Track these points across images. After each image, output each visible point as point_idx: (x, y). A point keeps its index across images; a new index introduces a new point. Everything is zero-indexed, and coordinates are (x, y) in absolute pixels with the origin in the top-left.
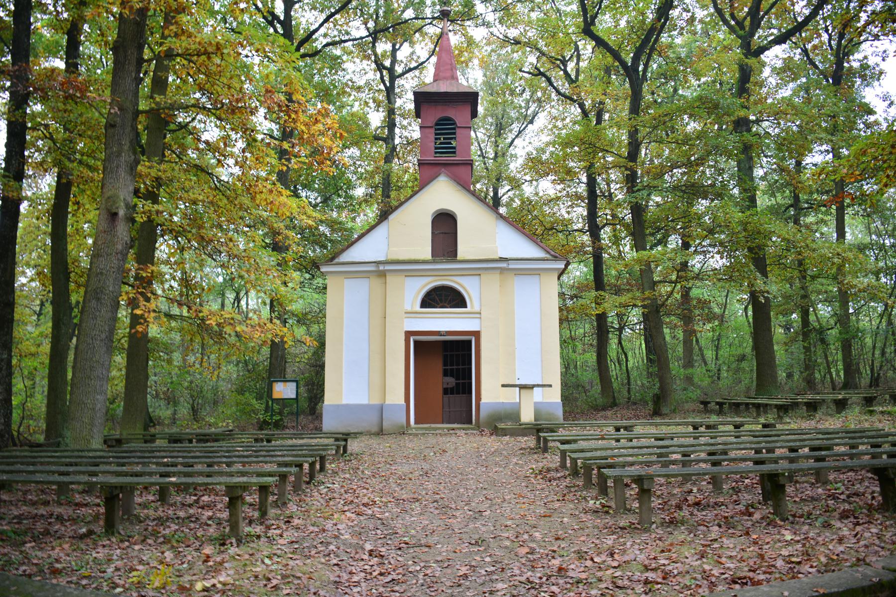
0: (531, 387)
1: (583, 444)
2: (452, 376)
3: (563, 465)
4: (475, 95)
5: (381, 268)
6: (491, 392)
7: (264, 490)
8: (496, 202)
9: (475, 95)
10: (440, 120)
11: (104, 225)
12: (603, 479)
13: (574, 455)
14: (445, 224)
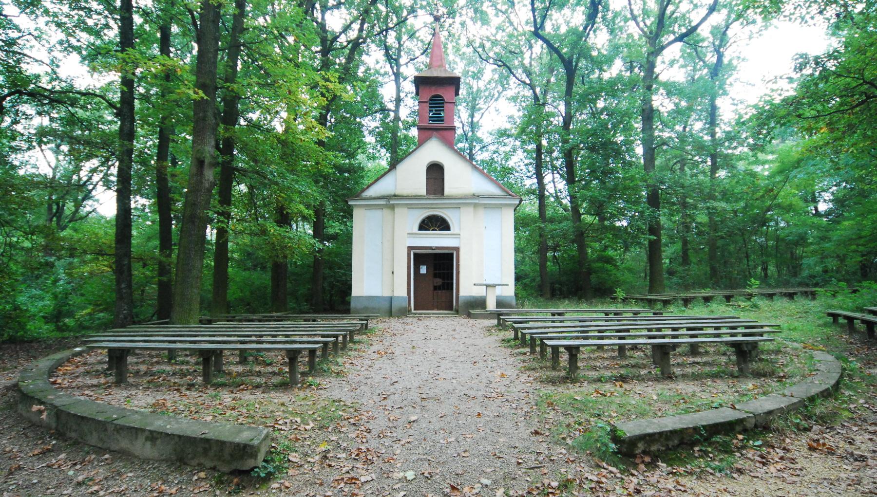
0: (494, 286)
1: (531, 324)
2: (440, 277)
3: (516, 338)
4: (458, 79)
5: (392, 202)
6: (468, 285)
7: (312, 352)
8: (472, 157)
9: (458, 79)
10: (433, 96)
11: (194, 170)
12: (543, 346)
13: (524, 331)
14: (435, 171)
